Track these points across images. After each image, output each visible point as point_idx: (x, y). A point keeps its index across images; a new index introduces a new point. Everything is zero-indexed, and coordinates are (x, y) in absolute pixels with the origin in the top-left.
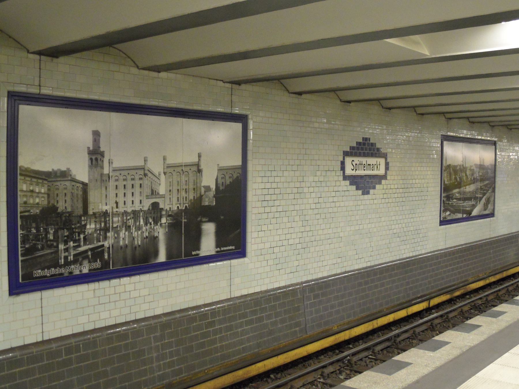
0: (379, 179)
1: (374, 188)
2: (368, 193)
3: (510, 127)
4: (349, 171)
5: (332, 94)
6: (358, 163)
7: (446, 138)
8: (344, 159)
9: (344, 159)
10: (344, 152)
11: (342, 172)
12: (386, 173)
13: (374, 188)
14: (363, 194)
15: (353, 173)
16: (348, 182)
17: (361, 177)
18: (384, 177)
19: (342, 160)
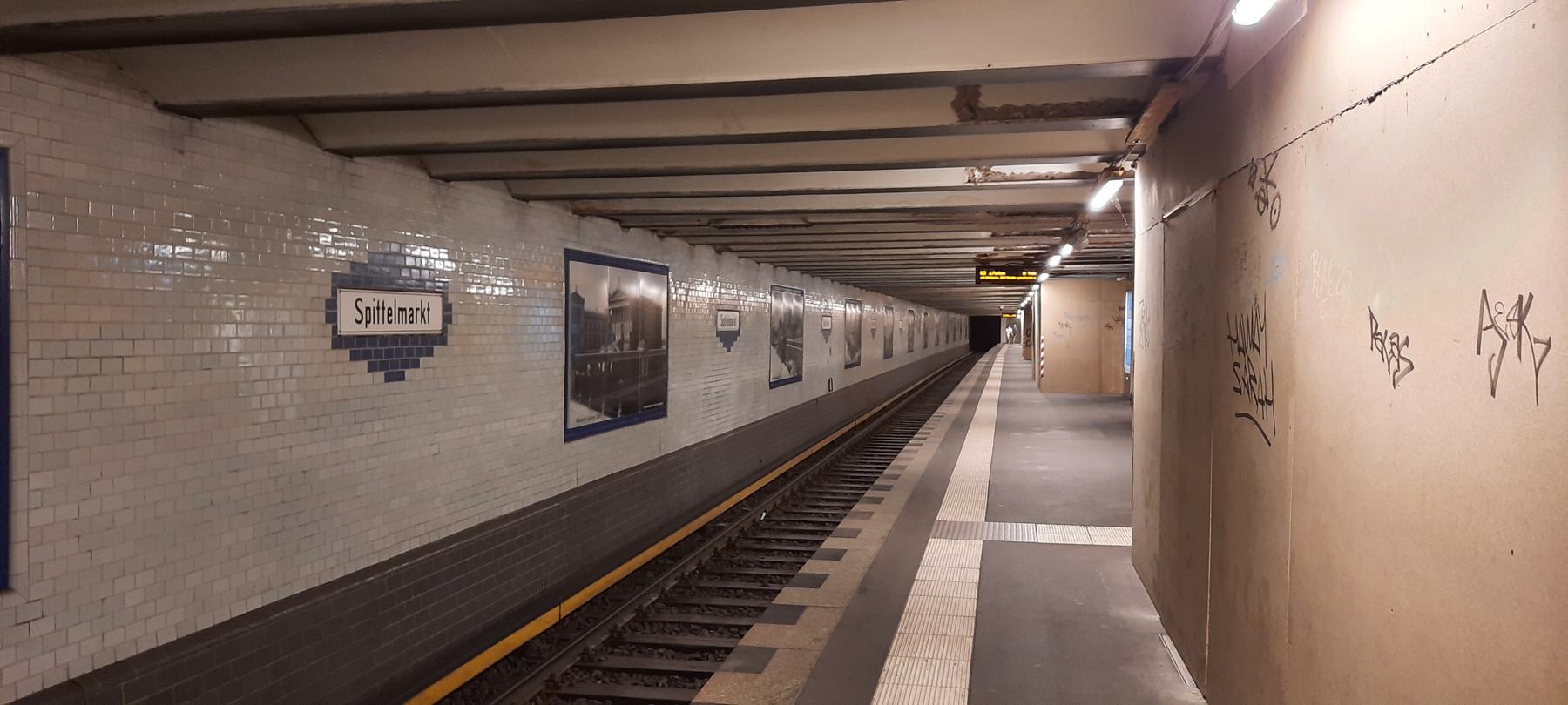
0: (425, 345)
1: (416, 365)
2: (401, 377)
3: (580, 205)
4: (435, 302)
5: (501, 184)
6: (373, 305)
7: (571, 255)
8: (334, 293)
9: (334, 293)
10: (567, 251)
11: (330, 326)
12: (444, 329)
13: (416, 365)
14: (389, 378)
15: (361, 329)
16: (345, 354)
17: (383, 339)
18: (441, 339)
19: (329, 295)
